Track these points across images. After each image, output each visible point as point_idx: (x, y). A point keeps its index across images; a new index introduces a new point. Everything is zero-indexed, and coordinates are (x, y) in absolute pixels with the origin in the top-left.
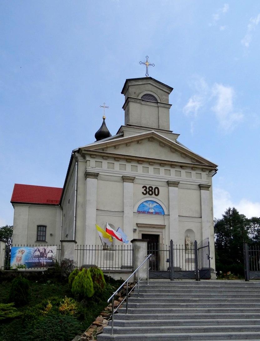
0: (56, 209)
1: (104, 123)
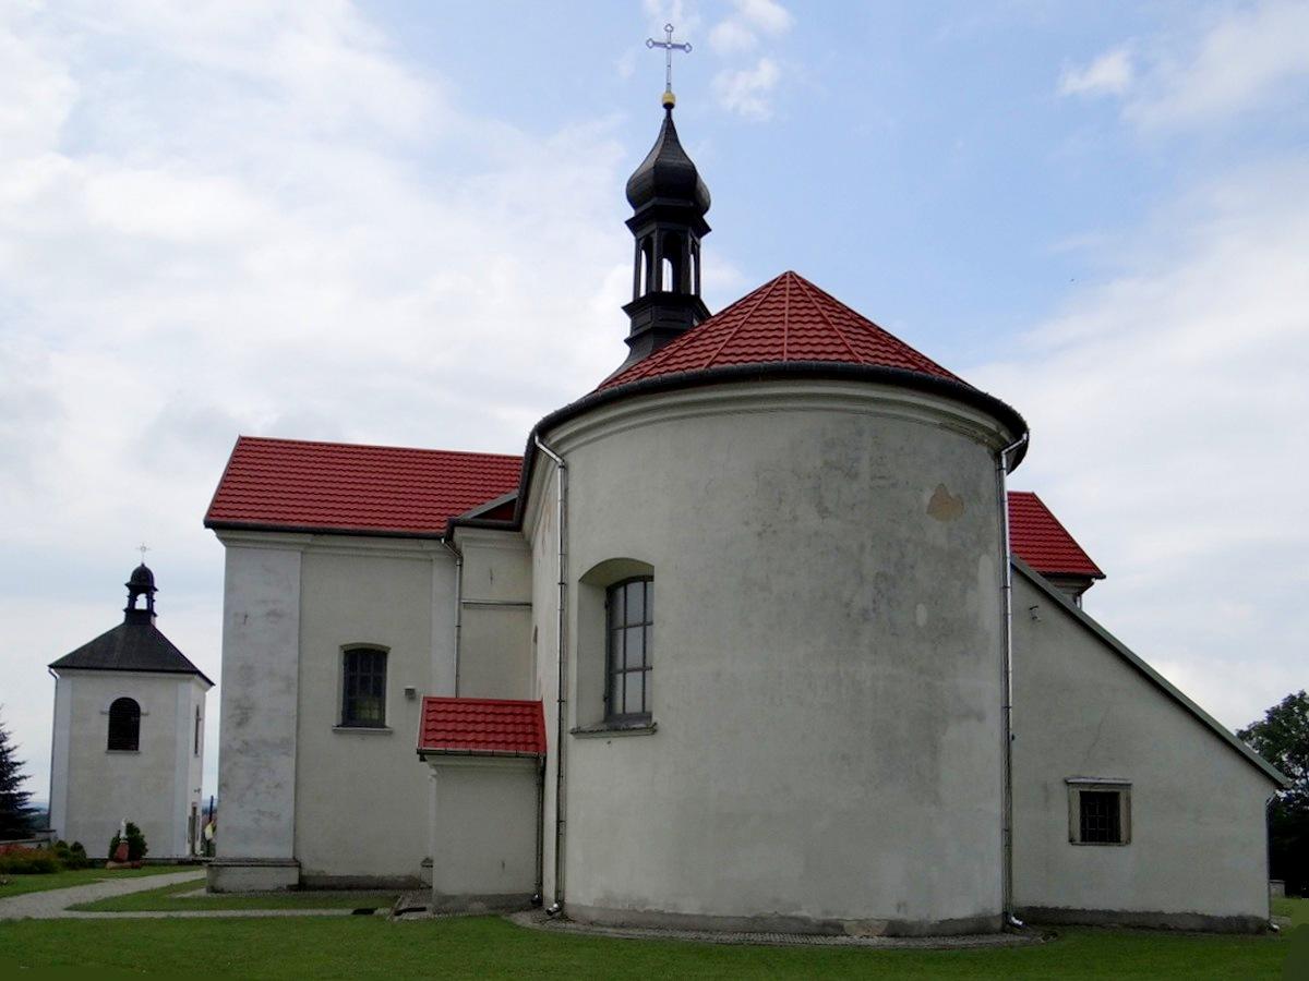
1: (669, 129)
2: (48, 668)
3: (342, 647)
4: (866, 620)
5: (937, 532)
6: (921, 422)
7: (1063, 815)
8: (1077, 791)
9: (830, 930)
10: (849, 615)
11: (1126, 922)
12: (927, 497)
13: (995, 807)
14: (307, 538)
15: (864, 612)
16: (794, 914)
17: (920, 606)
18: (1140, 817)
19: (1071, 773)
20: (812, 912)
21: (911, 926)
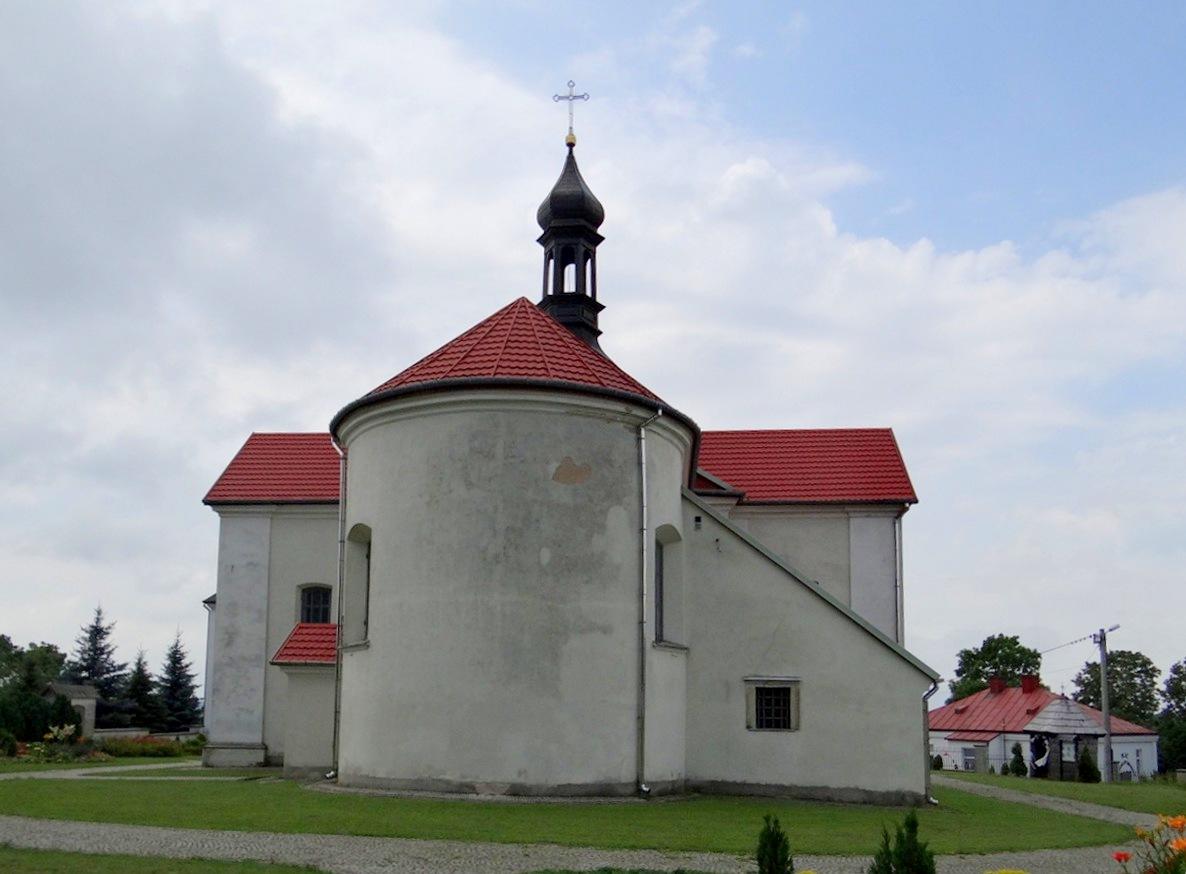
0: (848, 519)
1: (571, 162)
2: (203, 604)
3: (299, 586)
4: (498, 562)
5: (562, 494)
6: (549, 413)
7: (742, 707)
8: (753, 687)
9: (466, 789)
10: (485, 559)
11: (794, 794)
12: (553, 467)
13: (630, 699)
14: (274, 508)
15: (496, 556)
16: (441, 777)
17: (544, 549)
18: (807, 707)
19: (749, 672)
20: (453, 776)
21: (530, 788)
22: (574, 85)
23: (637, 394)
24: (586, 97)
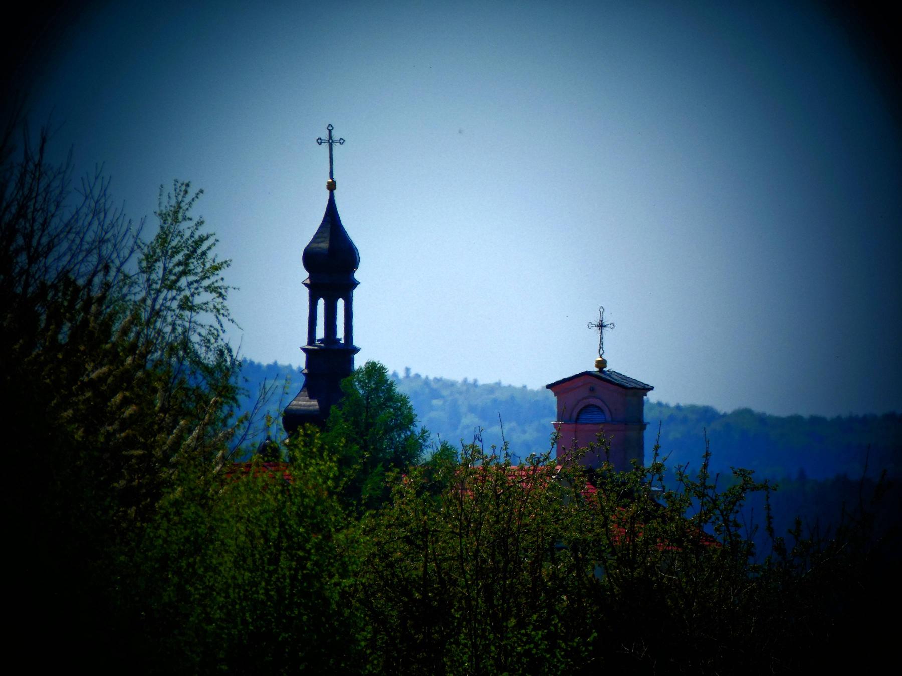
1: (332, 214)
22: (320, 138)
23: (634, 385)
24: (330, 128)
